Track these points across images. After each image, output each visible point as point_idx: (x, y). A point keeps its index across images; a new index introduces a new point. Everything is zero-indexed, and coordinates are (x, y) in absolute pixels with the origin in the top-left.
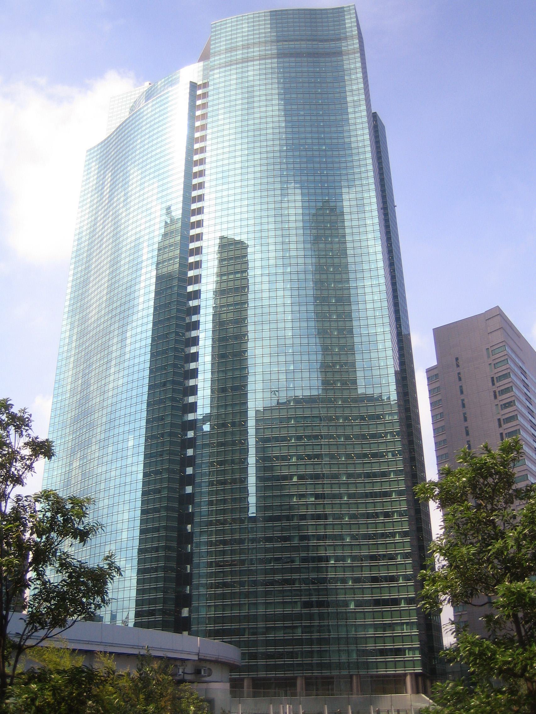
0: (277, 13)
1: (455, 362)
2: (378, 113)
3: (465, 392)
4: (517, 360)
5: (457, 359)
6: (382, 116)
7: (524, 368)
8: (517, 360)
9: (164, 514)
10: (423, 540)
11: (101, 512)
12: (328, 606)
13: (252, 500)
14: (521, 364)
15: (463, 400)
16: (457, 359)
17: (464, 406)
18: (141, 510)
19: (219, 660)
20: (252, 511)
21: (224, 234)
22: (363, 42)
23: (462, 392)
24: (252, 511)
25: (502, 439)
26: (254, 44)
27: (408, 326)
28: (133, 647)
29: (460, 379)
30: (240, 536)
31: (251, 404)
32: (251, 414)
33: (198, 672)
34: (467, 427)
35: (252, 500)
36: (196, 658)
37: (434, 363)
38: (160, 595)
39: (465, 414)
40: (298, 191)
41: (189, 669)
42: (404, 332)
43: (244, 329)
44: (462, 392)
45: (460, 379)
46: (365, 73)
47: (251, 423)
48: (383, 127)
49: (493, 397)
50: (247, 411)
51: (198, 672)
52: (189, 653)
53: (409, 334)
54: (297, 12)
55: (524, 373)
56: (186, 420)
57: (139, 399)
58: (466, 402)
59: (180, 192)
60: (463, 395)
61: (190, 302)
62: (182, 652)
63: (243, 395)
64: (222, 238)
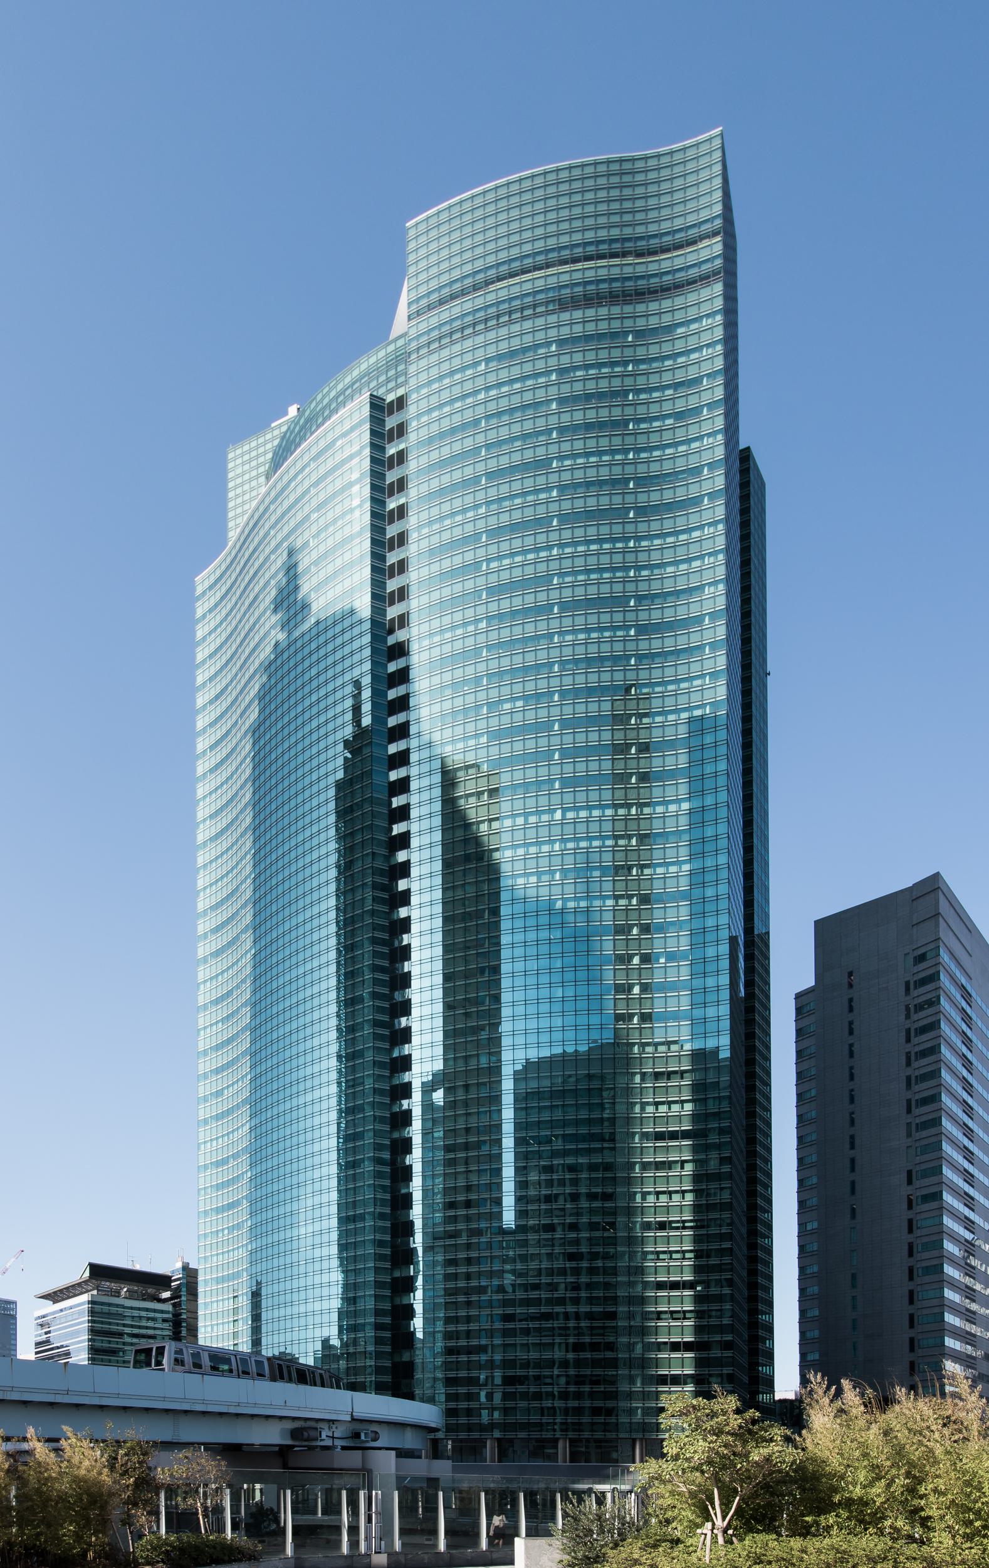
1: (845, 980)
3: (856, 1032)
4: (958, 974)
6: (760, 458)
7: (969, 988)
8: (958, 974)
11: (302, 1242)
12: (616, 1367)
13: (509, 1200)
14: (964, 981)
15: (851, 1045)
16: (850, 974)
17: (851, 1055)
20: (509, 1218)
22: (735, 262)
23: (851, 1032)
24: (509, 1218)
25: (909, 1111)
29: (851, 1009)
31: (506, 1056)
32: (507, 1071)
34: (852, 1090)
35: (509, 1200)
37: (811, 982)
39: (851, 1068)
40: (583, 1048)
42: (758, 929)
43: (495, 1116)
44: (851, 1032)
45: (851, 1009)
46: (731, 402)
47: (508, 1085)
48: (762, 485)
49: (903, 1040)
50: (501, 1124)
53: (768, 933)
55: (967, 996)
56: (395, 918)
58: (856, 1049)
59: (364, 670)
61: (395, 827)
63: (494, 1044)
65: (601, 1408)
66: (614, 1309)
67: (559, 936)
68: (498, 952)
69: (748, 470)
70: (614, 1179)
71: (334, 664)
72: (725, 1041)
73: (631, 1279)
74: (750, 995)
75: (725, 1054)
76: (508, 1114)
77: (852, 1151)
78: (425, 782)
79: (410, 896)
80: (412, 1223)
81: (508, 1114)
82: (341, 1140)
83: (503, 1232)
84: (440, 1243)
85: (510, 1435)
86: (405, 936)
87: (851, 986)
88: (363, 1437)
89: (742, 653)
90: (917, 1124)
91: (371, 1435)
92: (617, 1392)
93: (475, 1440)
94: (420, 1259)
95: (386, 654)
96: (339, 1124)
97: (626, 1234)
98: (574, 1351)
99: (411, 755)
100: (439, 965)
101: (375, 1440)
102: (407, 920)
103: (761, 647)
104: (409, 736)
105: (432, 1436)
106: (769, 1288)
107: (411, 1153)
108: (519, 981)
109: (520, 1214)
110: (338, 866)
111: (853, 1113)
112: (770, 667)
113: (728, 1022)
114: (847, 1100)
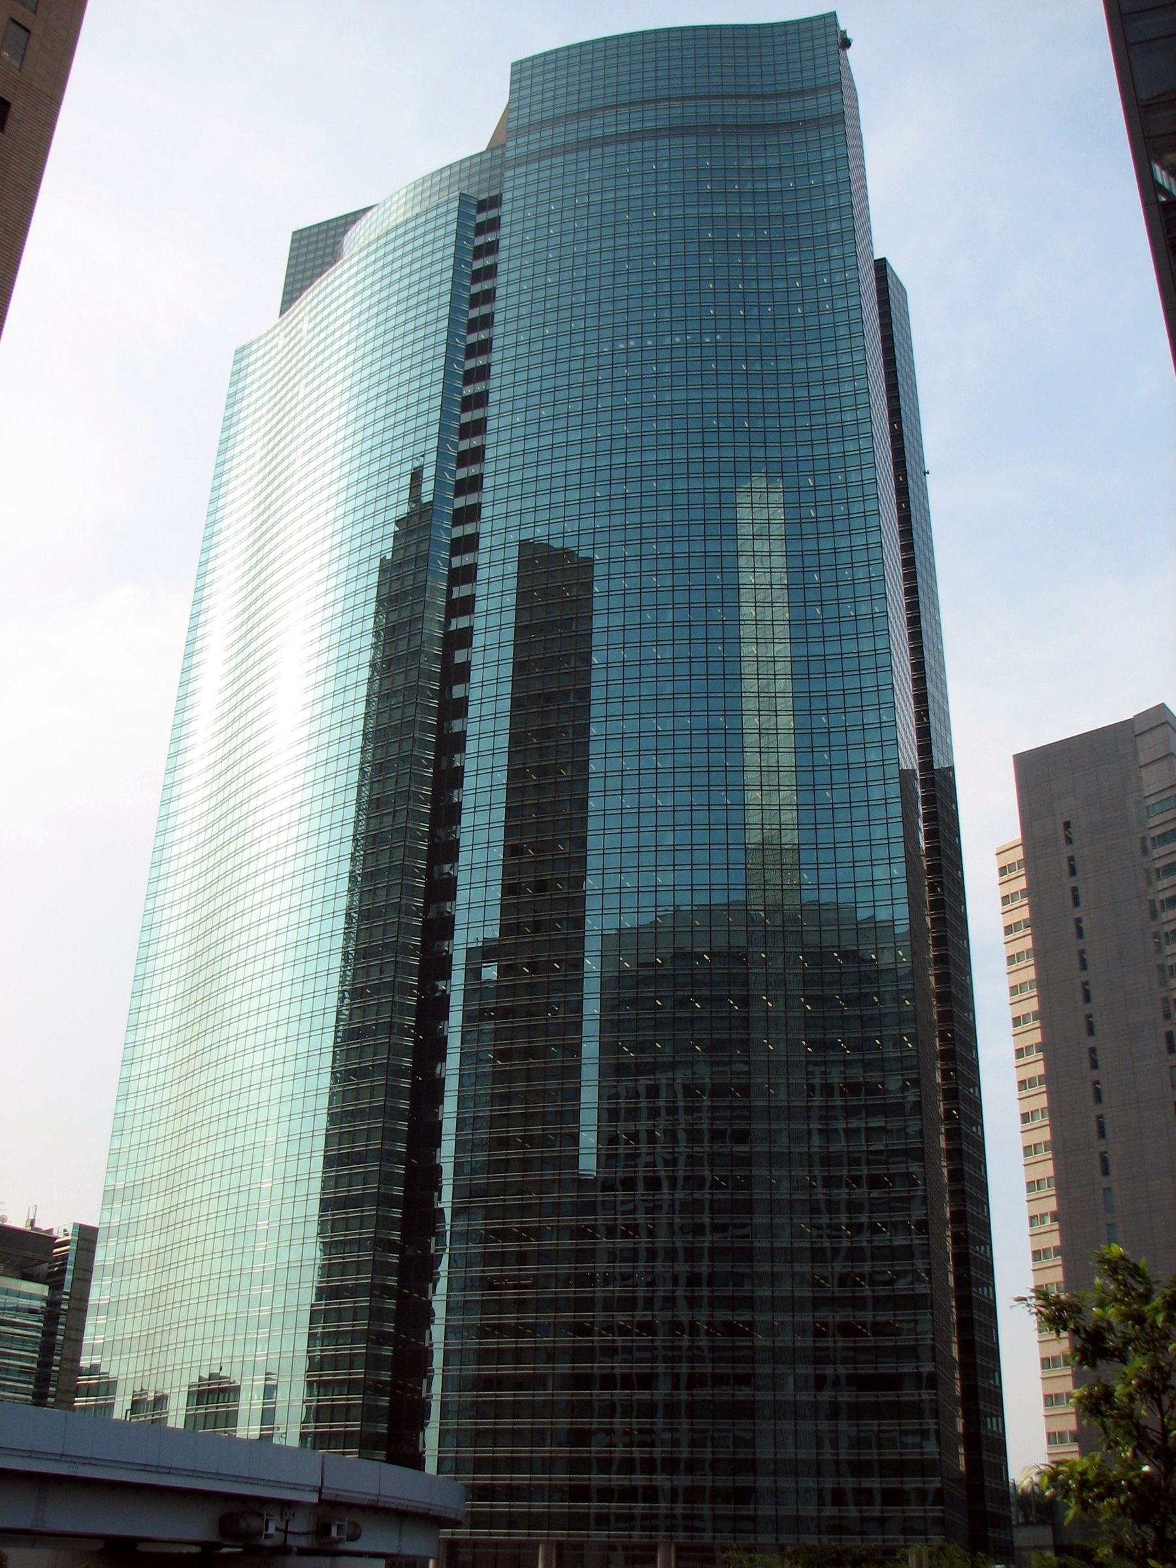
0: (608, 43)
1: (1061, 834)
2: (892, 262)
5: (1067, 825)
9: (373, 1166)
10: (966, 1242)
13: (589, 1139)
16: (1067, 825)
18: (325, 1157)
19: (381, 1504)
20: (588, 1163)
21: (527, 534)
24: (588, 1163)
26: (605, 108)
27: (949, 747)
28: (145, 1468)
30: (468, 1225)
32: (592, 944)
33: (322, 1530)
35: (589, 1139)
36: (314, 1498)
38: (361, 1348)
41: (300, 1523)
42: (939, 762)
48: (903, 291)
51: (322, 1530)
52: (295, 1487)
53: (952, 769)
54: (821, 22)
57: (329, 908)
60: (1078, 909)
61: (455, 590)
62: (276, 1484)
64: (523, 545)
65: (728, 1375)
66: (746, 1081)
67: (669, 802)
68: (586, 782)
69: (886, 278)
70: (749, 1178)
71: (392, 453)
72: (902, 911)
73: (774, 1126)
74: (934, 869)
75: (902, 928)
76: (592, 1008)
77: (1095, 1072)
78: (496, 571)
79: (472, 636)
80: (438, 1170)
81: (592, 1008)
82: (340, 1034)
83: (582, 1183)
84: (478, 1202)
85: (578, 1535)
86: (457, 756)
87: (1069, 841)
88: (334, 1533)
89: (893, 450)
90: (1162, 901)
91: (347, 1529)
92: (749, 1130)
93: (520, 1545)
94: (448, 1227)
95: (464, 352)
96: (339, 1013)
97: (766, 1104)
98: (689, 1387)
99: (492, 368)
100: (499, 834)
101: (353, 1538)
102: (462, 735)
103: (924, 524)
104: (477, 549)
105: (446, 1533)
106: (991, 1328)
107: (444, 1060)
108: (613, 822)
109: (606, 1159)
110: (373, 665)
111: (1098, 1083)
112: (928, 467)
113: (904, 887)
114: (1080, 996)
